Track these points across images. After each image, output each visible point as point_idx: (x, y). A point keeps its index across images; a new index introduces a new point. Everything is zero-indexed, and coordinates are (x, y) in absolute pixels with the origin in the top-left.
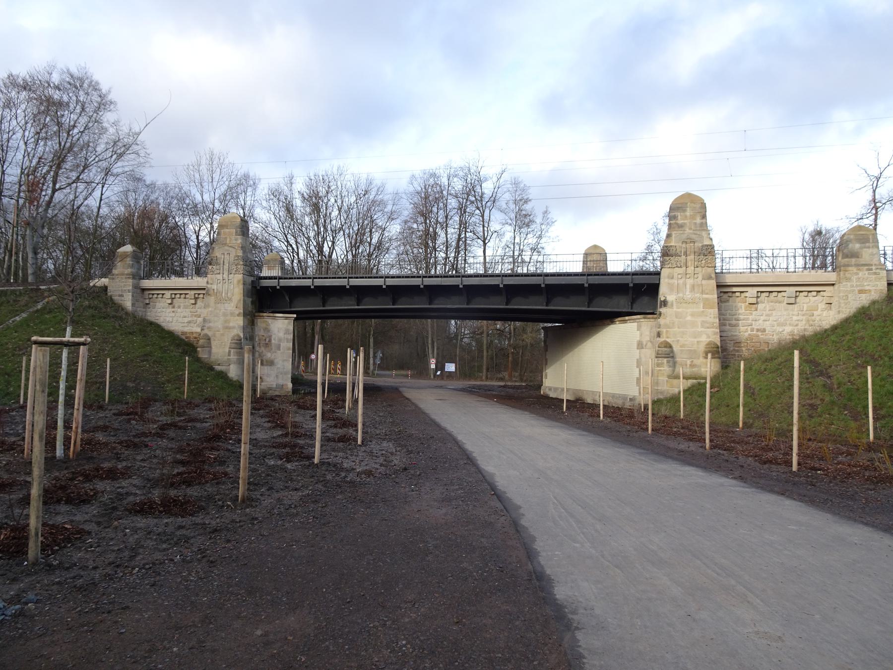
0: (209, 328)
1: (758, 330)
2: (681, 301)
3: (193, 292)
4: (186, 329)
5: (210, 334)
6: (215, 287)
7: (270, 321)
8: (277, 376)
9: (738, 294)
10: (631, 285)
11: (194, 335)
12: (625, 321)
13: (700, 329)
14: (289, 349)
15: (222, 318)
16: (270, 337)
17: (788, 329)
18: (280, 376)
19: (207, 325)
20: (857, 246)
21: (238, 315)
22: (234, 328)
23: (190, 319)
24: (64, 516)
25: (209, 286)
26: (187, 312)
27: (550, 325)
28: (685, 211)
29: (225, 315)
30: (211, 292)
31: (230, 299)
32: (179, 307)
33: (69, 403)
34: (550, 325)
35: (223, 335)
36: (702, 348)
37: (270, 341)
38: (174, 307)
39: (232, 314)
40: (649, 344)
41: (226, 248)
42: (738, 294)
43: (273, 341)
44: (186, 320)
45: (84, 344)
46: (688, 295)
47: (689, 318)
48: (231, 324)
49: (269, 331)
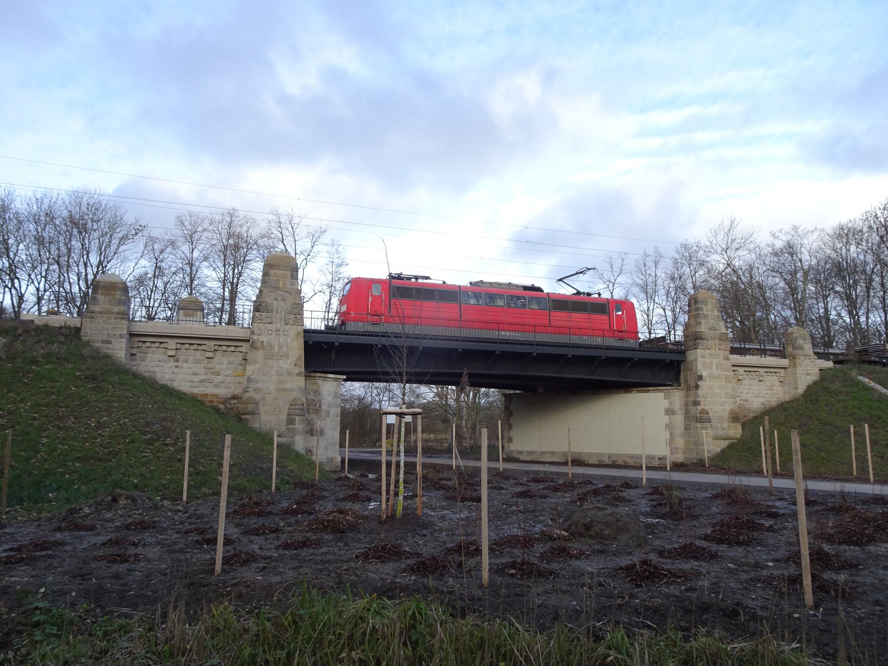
0: (255, 390)
1: (744, 400)
2: (712, 377)
3: (212, 343)
4: (196, 391)
5: (257, 397)
6: (264, 339)
7: (320, 382)
8: (326, 448)
9: (148, 344)
10: (337, 344)
11: (210, 398)
12: (648, 391)
13: (725, 400)
14: (337, 416)
15: (275, 378)
16: (320, 401)
17: (761, 400)
18: (329, 448)
19: (253, 386)
20: (802, 341)
21: (299, 374)
22: (292, 390)
23: (204, 377)
24: (791, 570)
25: (255, 337)
26: (200, 368)
27: (512, 392)
28: (707, 305)
29: (279, 374)
30: (259, 345)
31: (287, 356)
32: (187, 361)
33: (397, 481)
34: (512, 392)
35: (276, 398)
36: (726, 415)
37: (320, 406)
38: (177, 361)
39: (289, 373)
40: (680, 412)
41: (280, 292)
42: (187, 346)
43: (323, 407)
44: (197, 378)
45: (419, 414)
46: (715, 372)
47: (717, 390)
48: (288, 386)
49: (319, 394)
